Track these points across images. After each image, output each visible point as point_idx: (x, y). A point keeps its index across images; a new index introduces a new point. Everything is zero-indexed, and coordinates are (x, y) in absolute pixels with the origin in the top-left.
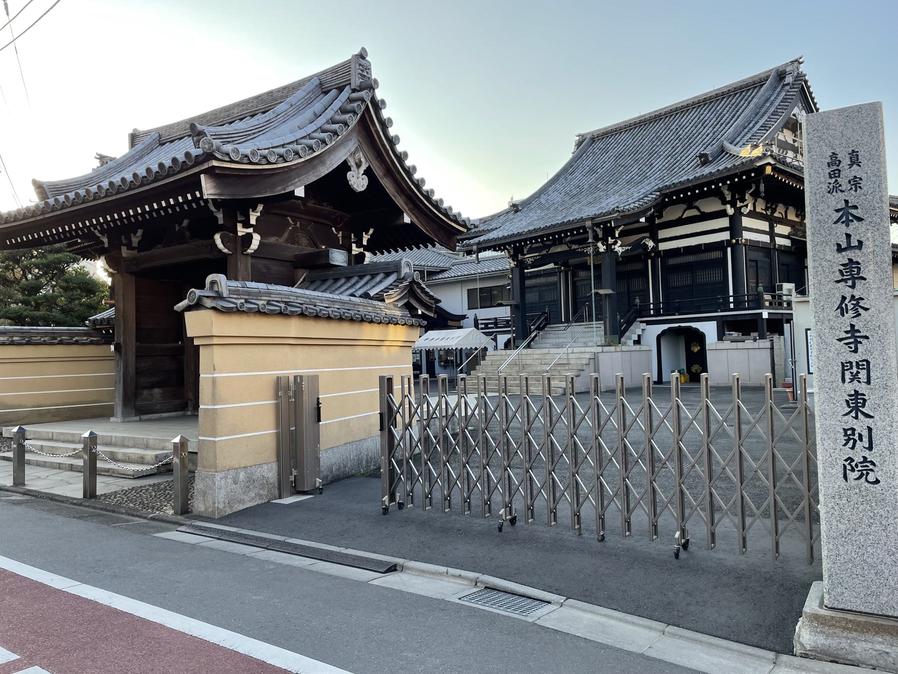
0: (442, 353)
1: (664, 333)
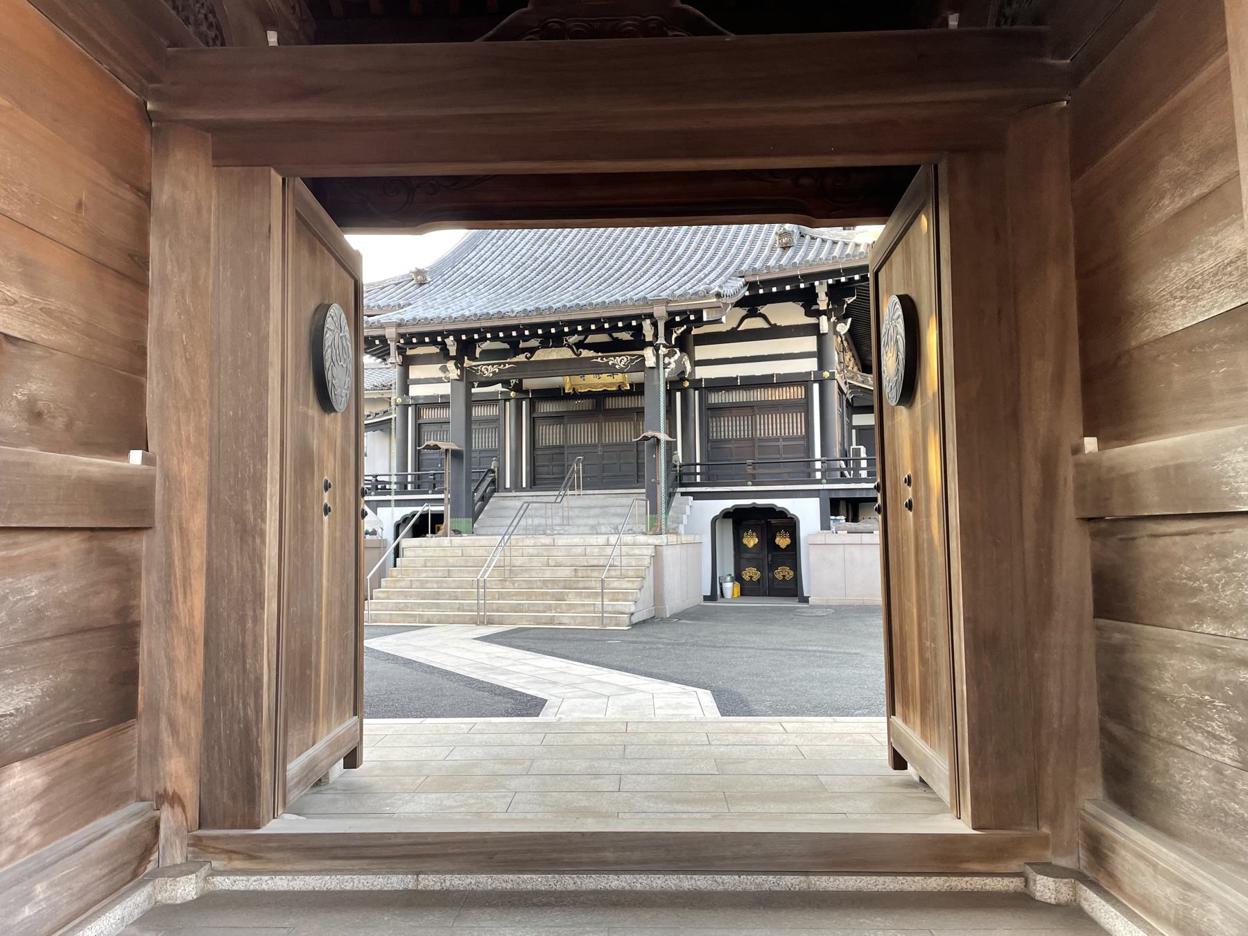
1: (726, 514)
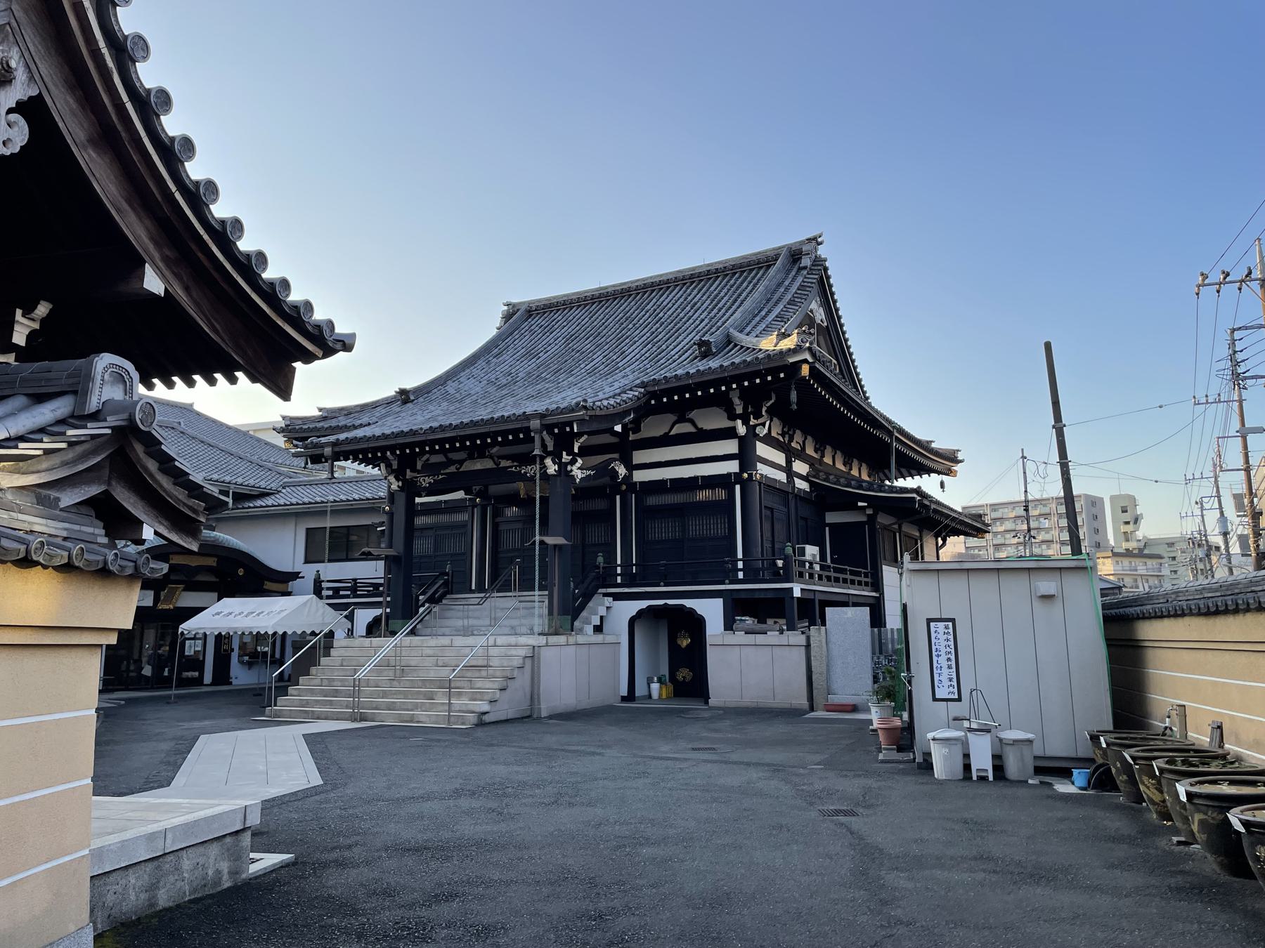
0: (247, 639)
1: (641, 613)
